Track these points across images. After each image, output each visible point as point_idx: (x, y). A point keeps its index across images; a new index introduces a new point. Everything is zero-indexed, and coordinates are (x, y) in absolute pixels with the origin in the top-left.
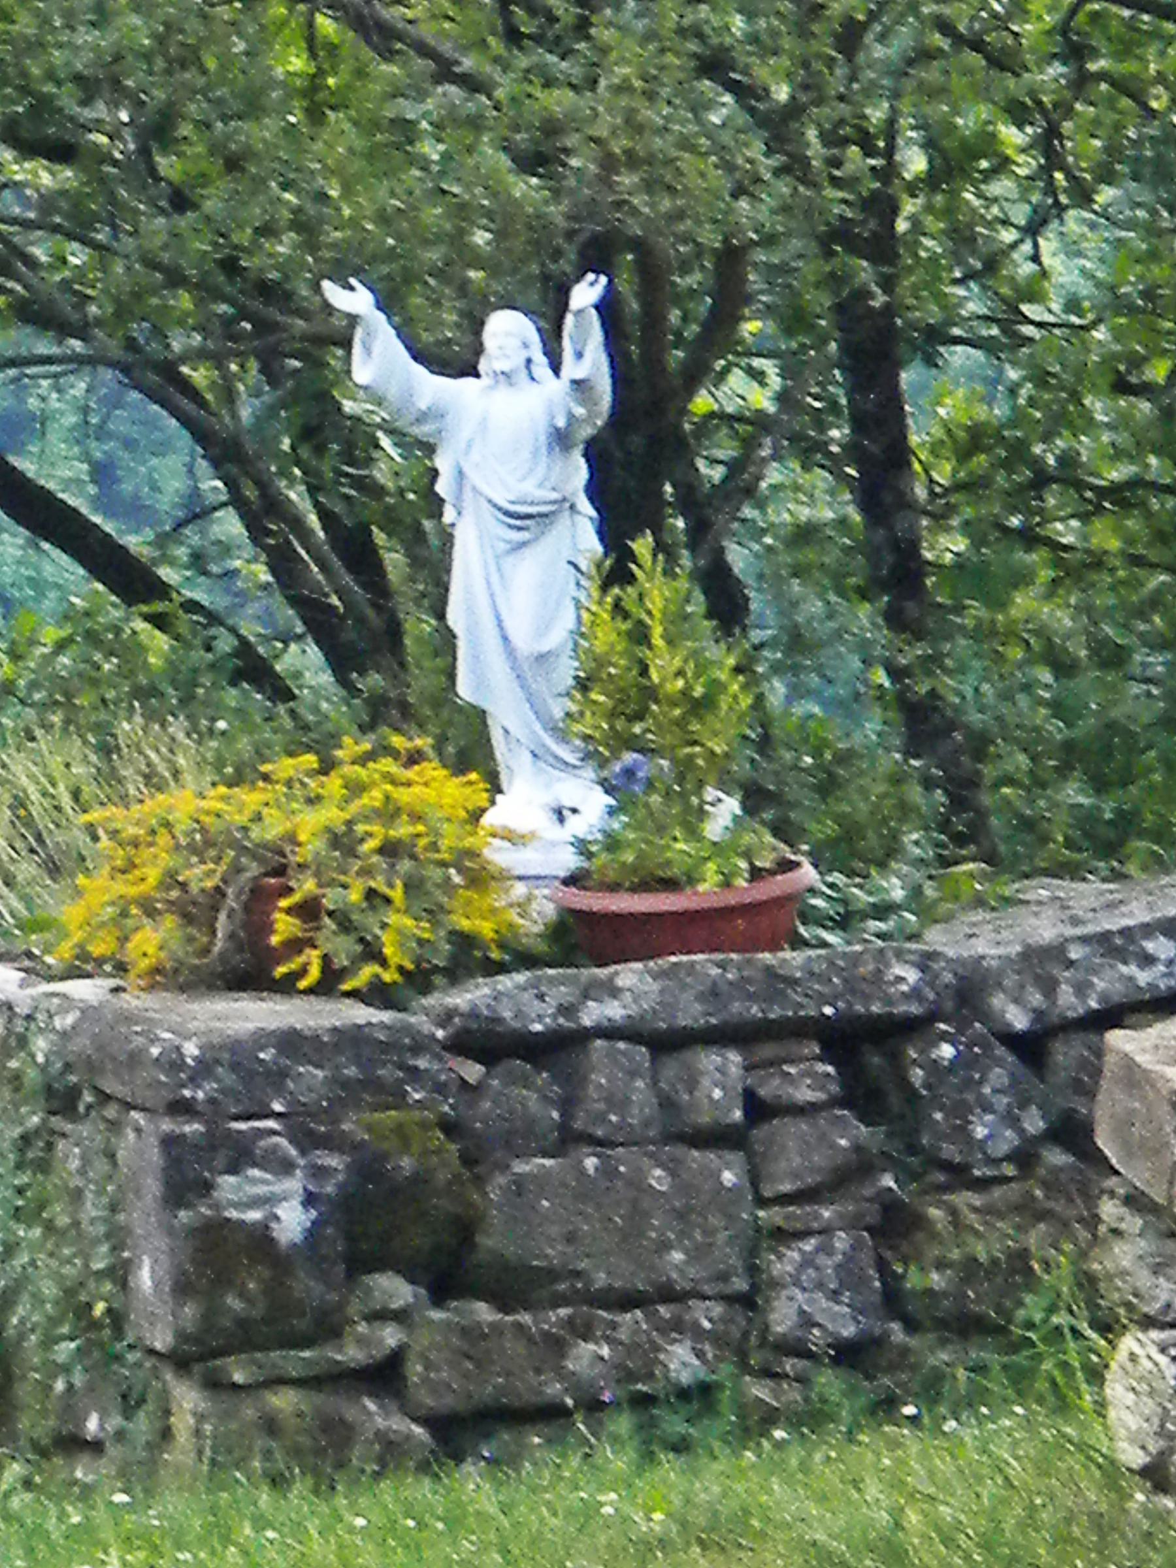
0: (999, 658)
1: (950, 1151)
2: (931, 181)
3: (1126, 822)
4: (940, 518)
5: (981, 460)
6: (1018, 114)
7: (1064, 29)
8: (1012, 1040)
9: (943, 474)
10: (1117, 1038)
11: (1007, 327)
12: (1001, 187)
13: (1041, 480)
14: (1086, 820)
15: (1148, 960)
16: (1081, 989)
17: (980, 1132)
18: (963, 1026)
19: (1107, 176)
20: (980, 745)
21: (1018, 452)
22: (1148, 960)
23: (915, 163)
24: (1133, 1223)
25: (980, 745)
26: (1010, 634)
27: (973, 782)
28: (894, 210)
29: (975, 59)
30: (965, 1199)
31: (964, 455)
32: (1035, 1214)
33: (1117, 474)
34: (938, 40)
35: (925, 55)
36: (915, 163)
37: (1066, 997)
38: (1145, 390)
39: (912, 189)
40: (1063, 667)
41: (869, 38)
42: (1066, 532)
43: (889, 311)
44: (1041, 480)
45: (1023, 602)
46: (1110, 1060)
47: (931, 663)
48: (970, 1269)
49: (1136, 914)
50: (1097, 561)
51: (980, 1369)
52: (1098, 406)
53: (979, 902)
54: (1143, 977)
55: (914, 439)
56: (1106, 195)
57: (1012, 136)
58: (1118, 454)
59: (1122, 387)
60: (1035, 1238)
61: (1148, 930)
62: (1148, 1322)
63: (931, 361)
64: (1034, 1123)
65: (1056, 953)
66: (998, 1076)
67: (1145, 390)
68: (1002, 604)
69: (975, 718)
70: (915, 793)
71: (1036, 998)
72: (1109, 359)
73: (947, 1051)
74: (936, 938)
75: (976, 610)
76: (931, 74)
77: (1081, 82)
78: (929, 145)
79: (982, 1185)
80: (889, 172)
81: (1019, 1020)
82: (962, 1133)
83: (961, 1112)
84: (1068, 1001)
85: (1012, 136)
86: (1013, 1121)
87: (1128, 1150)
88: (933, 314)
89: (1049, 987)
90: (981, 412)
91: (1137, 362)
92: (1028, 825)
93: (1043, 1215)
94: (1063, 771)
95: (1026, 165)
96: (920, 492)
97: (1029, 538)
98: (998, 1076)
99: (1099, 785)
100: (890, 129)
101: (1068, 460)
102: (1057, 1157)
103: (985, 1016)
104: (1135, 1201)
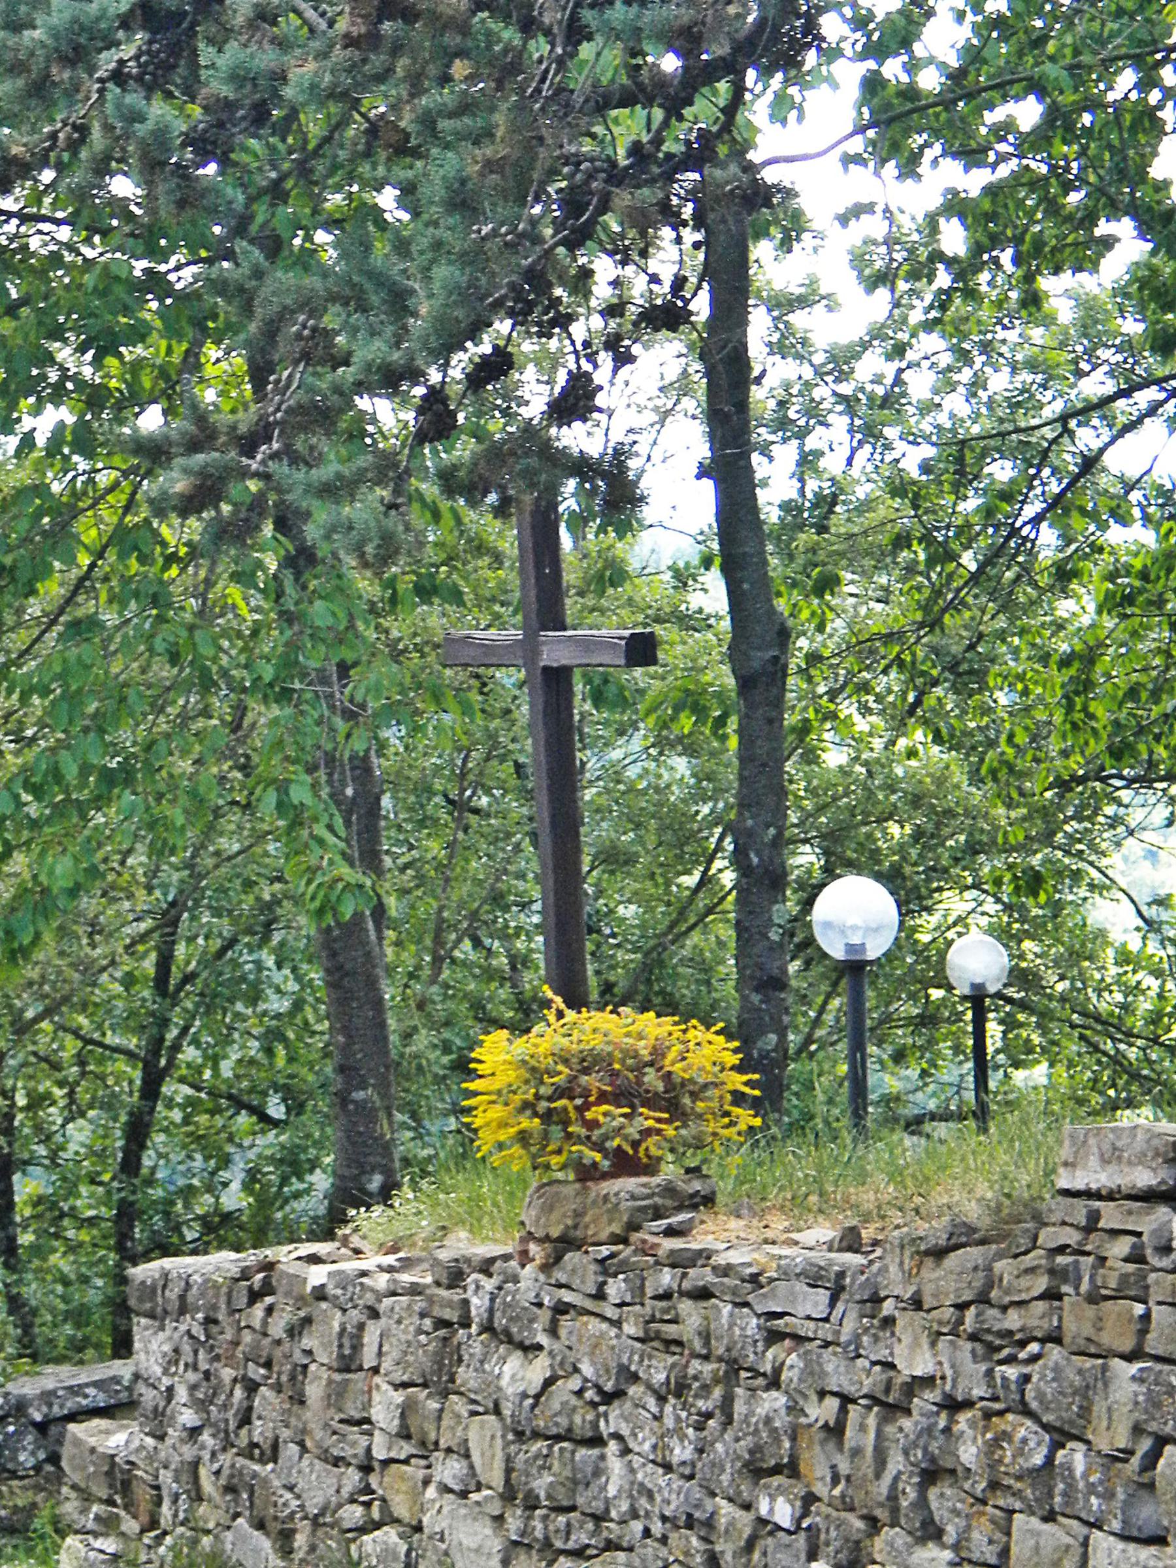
0: (44, 1280)
1: (10, 1466)
2: (28, 1108)
3: (86, 1339)
4: (25, 1228)
5: (40, 1208)
6: (61, 1084)
7: (79, 1054)
8: (35, 1424)
9: (28, 1212)
10: (72, 1427)
11: (53, 1161)
12: (52, 1110)
13: (62, 1215)
14: (71, 1339)
15: (86, 1396)
16: (62, 1407)
17: (22, 1458)
18: (17, 1419)
19: (91, 1107)
20: (34, 1312)
21: (54, 1205)
22: (86, 1396)
23: (21, 1101)
24: (73, 1495)
25: (34, 1312)
26: (48, 1271)
27: (31, 1325)
28: (13, 1117)
29: (44, 1065)
30: (15, 1483)
31: (35, 1205)
32: (38, 1488)
33: (91, 1213)
34: (33, 1059)
35: (25, 1064)
36: (21, 1101)
37: (56, 1409)
38: (101, 1184)
39: (21, 1109)
40: (66, 1283)
41: (375, 760)
42: (70, 1234)
43: (10, 1155)
44: (62, 1215)
45: (54, 1259)
46: (68, 1436)
47: (19, 1282)
48: (16, 1509)
49: (83, 1379)
50: (81, 1244)
51: (15, 1547)
52: (84, 1190)
53: (27, 1373)
54: (84, 1402)
55: (17, 1199)
56: (91, 1113)
57: (58, 1092)
58: (90, 1207)
59: (93, 1182)
60: (40, 1498)
61: (87, 1385)
62: (77, 1532)
63: (24, 1173)
64: (42, 1455)
65: (53, 1393)
66: (30, 1438)
67: (101, 1184)
68: (45, 1260)
69: (33, 1303)
70: (10, 1329)
71: (45, 1409)
72: (88, 1174)
73: (11, 1429)
74: (10, 1387)
75: (36, 1263)
76: (30, 1070)
77: (83, 1074)
78: (28, 1095)
79: (22, 1478)
80: (13, 1105)
81: (38, 1417)
82: (14, 1459)
83: (15, 1451)
84: (56, 1411)
85: (58, 1092)
86: (33, 1453)
87: (74, 1469)
88: (26, 1156)
89: (50, 1405)
90: (41, 1191)
91: (99, 1174)
92: (50, 1341)
93: (43, 1489)
94: (65, 1320)
95: (62, 1103)
96: (18, 1219)
97: (57, 1236)
98: (30, 1438)
99: (78, 1326)
100: (14, 1089)
101: (73, 1208)
102: (49, 1468)
103: (26, 1416)
104: (74, 1487)
